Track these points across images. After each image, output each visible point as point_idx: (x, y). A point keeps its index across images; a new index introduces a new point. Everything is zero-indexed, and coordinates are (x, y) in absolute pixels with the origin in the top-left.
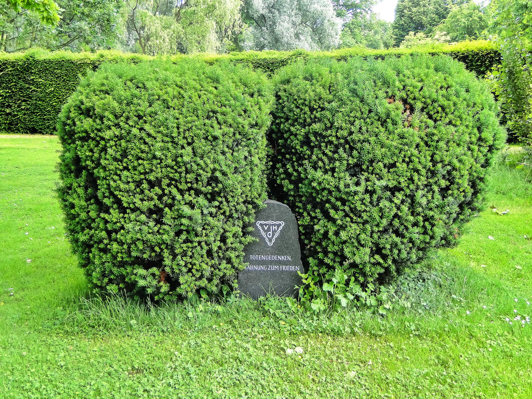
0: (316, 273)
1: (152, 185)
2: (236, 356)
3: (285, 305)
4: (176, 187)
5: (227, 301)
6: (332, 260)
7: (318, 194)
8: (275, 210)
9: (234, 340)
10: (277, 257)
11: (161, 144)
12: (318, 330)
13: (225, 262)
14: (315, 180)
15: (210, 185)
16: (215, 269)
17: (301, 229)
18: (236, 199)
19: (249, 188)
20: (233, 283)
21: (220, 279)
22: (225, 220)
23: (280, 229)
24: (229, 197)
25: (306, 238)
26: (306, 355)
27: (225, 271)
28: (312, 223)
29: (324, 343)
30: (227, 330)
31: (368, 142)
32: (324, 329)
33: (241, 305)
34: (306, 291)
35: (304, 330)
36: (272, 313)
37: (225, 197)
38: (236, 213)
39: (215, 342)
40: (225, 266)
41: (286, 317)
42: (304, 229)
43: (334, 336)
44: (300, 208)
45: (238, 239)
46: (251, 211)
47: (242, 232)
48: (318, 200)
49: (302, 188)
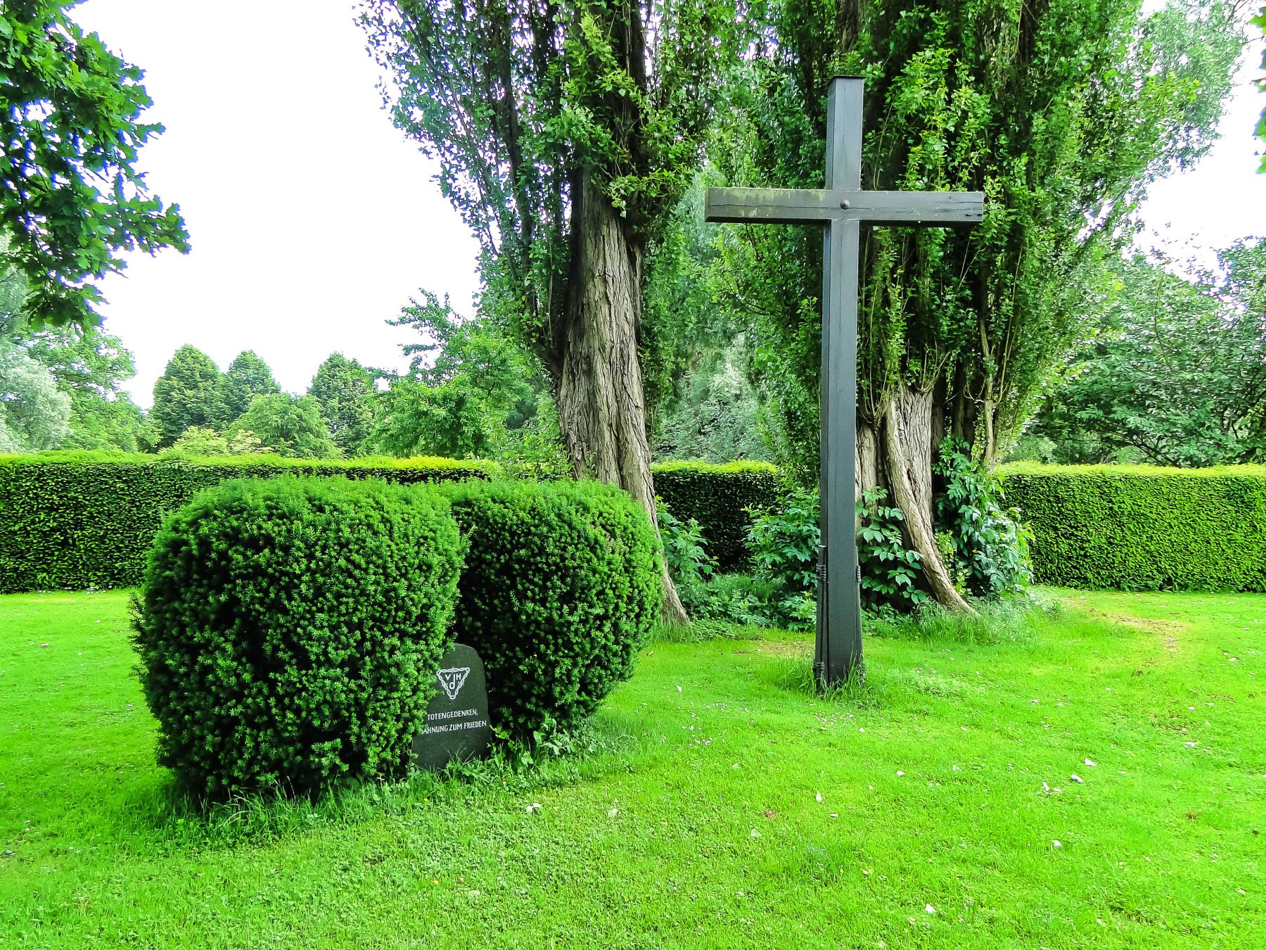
1: (352, 627)
4: (380, 629)
11: (373, 577)
31: (581, 568)
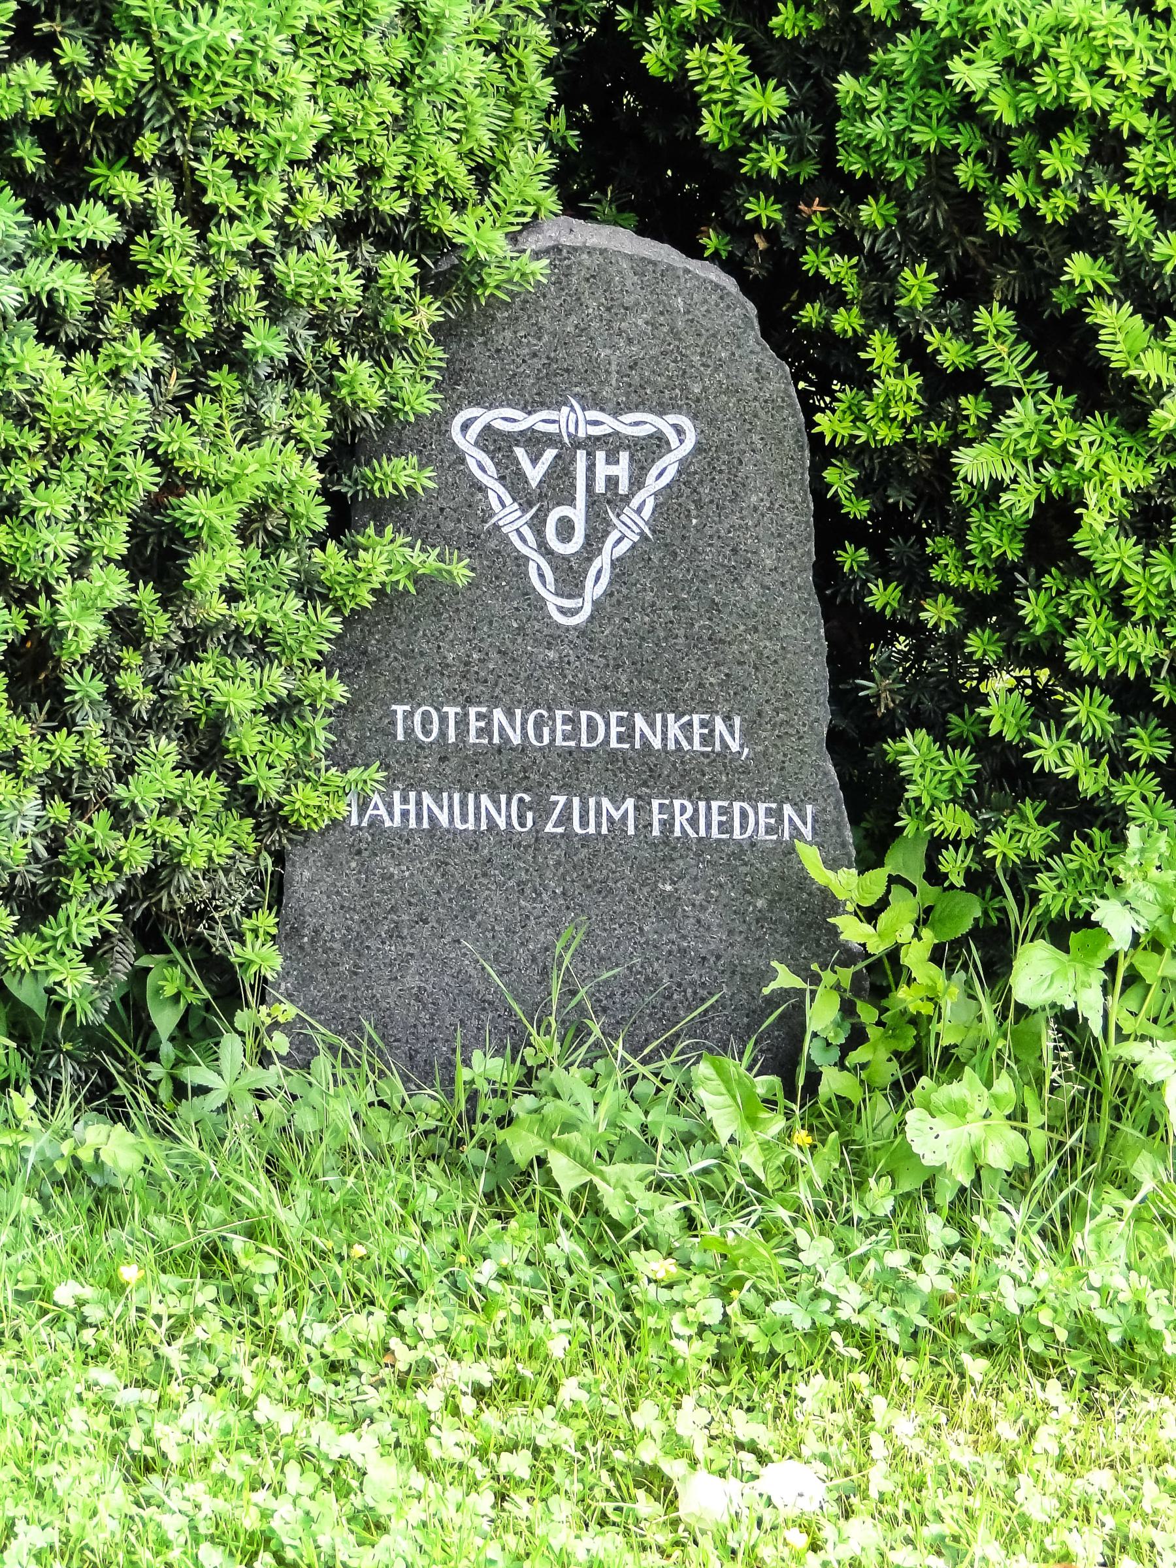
0: (954, 864)
2: (251, 1522)
3: (681, 1124)
5: (180, 1090)
6: (1095, 749)
7: (1002, 169)
8: (614, 308)
9: (242, 1402)
10: (627, 723)
12: (955, 1328)
13: (167, 748)
14: (978, 37)
15: (45, 49)
16: (80, 808)
17: (839, 478)
18: (273, 194)
19: (387, 99)
20: (239, 937)
21: (122, 902)
22: (173, 386)
23: (654, 483)
24: (211, 170)
25: (884, 569)
26: (852, 1527)
27: (171, 829)
28: (936, 434)
29: (1006, 1430)
30: (181, 1324)
32: (1007, 1322)
33: (306, 1121)
34: (867, 1013)
35: (842, 1327)
36: (567, 1187)
37: (171, 164)
38: (275, 319)
39: (77, 1415)
40: (174, 784)
41: (691, 1223)
42: (862, 488)
43: (1091, 1382)
44: (836, 298)
45: (287, 561)
46: (410, 308)
47: (327, 494)
48: (999, 220)
49: (864, 113)
